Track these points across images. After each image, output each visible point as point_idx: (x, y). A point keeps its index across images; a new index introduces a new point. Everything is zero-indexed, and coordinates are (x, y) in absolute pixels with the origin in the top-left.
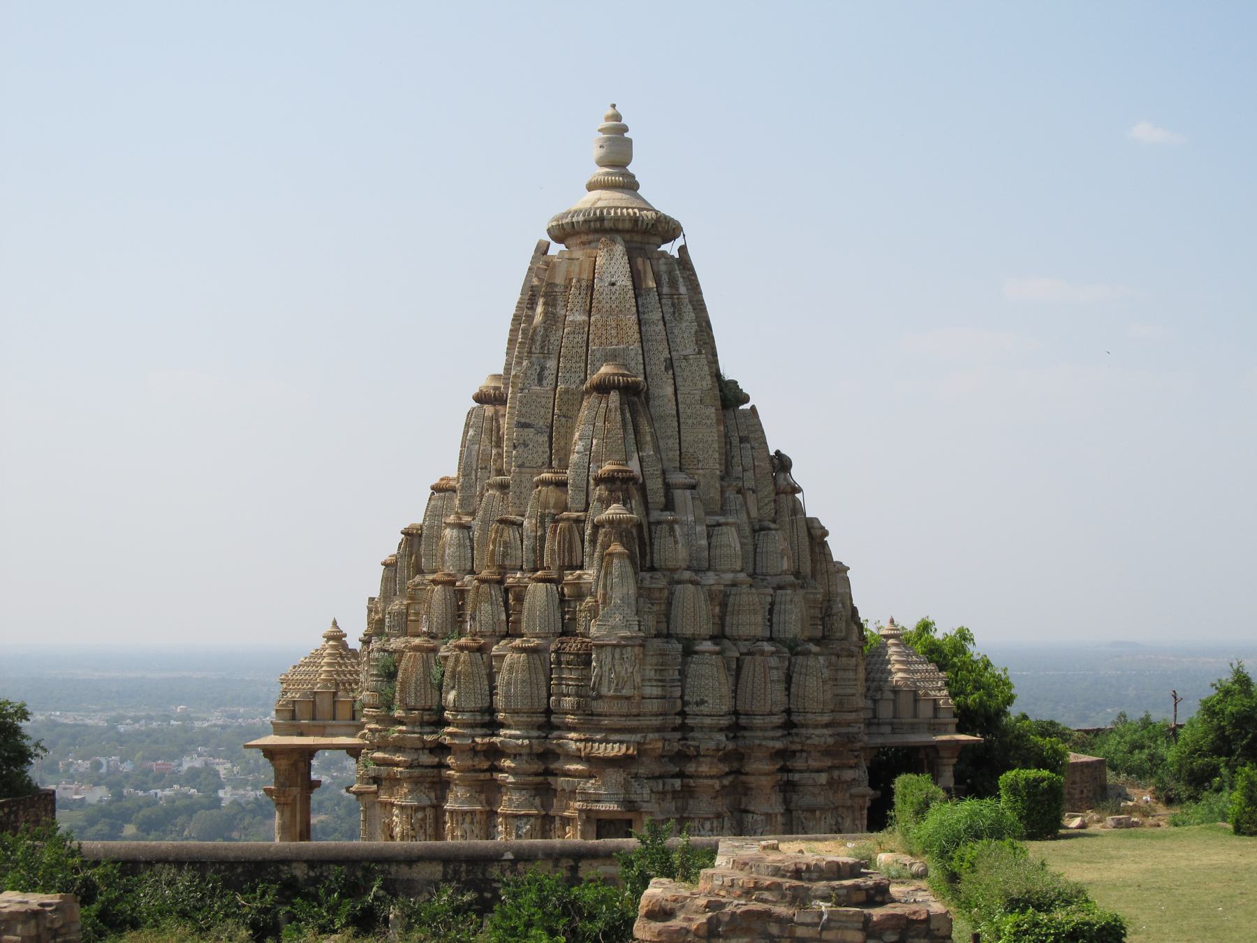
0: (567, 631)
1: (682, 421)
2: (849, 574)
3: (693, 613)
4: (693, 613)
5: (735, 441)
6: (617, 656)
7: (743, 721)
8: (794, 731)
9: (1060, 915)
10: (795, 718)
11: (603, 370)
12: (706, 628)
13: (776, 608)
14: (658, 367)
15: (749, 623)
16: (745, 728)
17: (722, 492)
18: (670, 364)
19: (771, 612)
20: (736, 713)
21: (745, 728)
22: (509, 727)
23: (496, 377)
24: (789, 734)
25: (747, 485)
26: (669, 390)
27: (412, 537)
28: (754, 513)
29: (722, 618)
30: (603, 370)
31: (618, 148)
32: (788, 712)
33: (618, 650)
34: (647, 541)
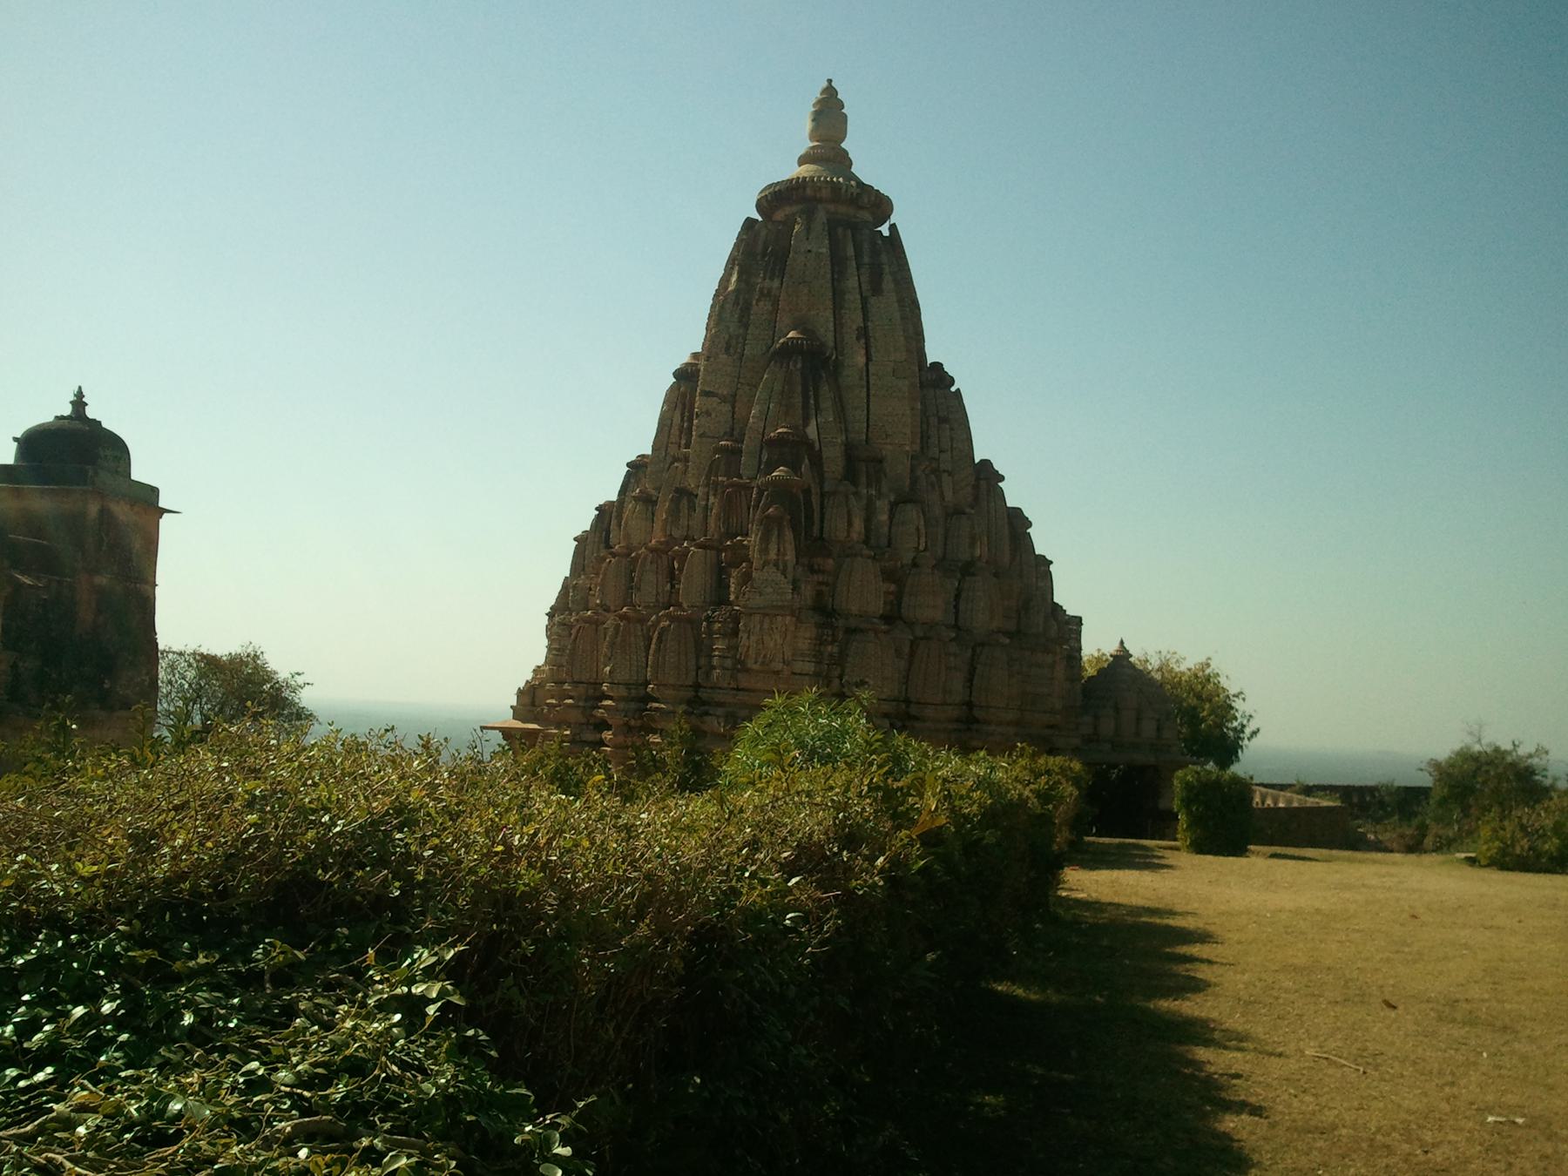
0: (721, 600)
1: (872, 392)
2: (1052, 568)
3: (863, 592)
4: (863, 592)
5: (933, 421)
6: (766, 626)
7: (913, 710)
8: (975, 726)
9: (1463, 855)
10: (977, 713)
11: (790, 335)
12: (877, 606)
13: (964, 595)
14: (850, 336)
15: (929, 606)
16: (916, 718)
17: (912, 470)
18: (864, 334)
19: (957, 597)
20: (907, 701)
21: (916, 718)
22: (656, 700)
23: (695, 355)
24: (969, 729)
25: (942, 466)
26: (861, 360)
27: (604, 511)
28: (949, 495)
29: (899, 596)
30: (790, 335)
31: (829, 113)
32: (970, 705)
33: (767, 620)
34: (817, 516)
